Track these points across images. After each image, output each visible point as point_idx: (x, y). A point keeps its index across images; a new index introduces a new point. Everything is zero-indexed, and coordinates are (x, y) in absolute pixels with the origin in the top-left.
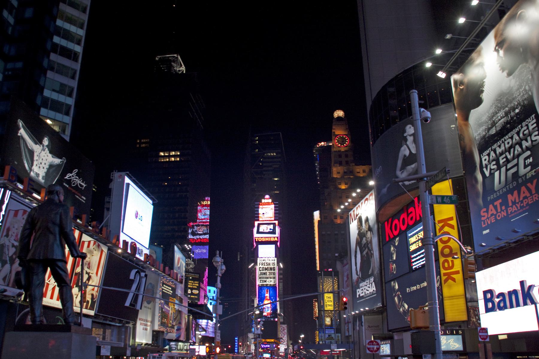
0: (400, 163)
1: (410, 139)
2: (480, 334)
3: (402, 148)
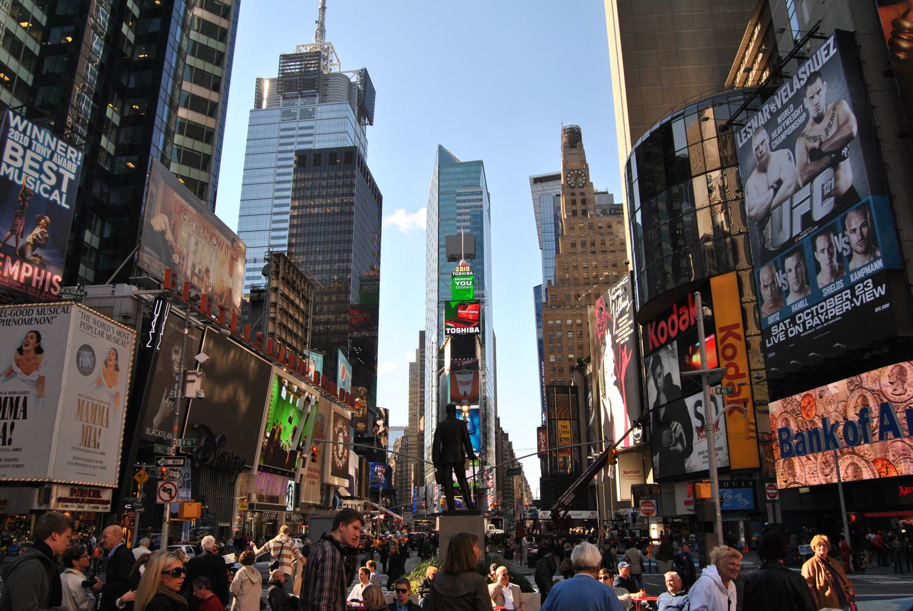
2: (769, 491)
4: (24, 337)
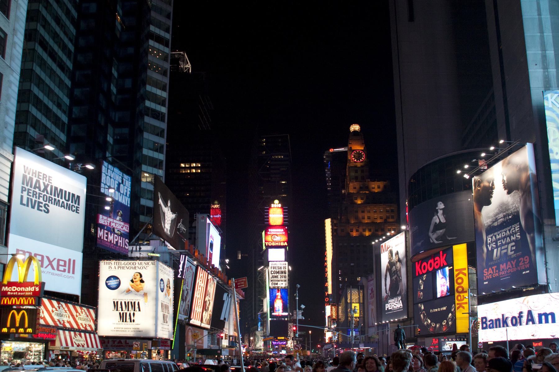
0: (432, 227)
1: (440, 212)
3: (434, 218)
4: (133, 275)
